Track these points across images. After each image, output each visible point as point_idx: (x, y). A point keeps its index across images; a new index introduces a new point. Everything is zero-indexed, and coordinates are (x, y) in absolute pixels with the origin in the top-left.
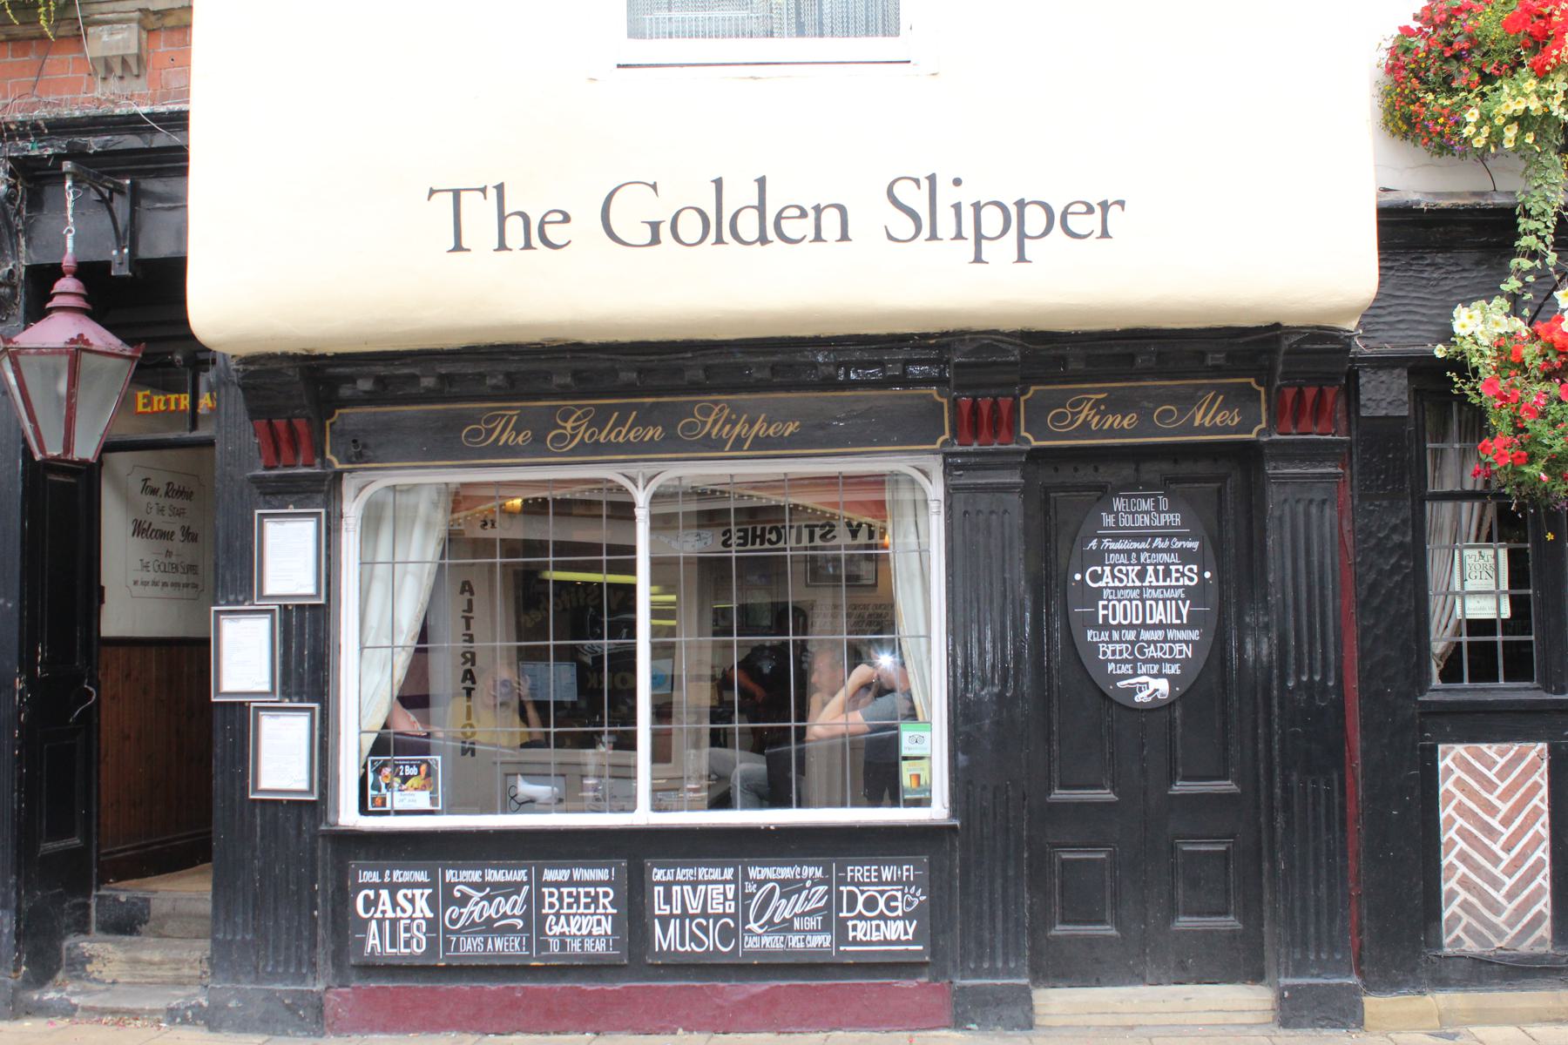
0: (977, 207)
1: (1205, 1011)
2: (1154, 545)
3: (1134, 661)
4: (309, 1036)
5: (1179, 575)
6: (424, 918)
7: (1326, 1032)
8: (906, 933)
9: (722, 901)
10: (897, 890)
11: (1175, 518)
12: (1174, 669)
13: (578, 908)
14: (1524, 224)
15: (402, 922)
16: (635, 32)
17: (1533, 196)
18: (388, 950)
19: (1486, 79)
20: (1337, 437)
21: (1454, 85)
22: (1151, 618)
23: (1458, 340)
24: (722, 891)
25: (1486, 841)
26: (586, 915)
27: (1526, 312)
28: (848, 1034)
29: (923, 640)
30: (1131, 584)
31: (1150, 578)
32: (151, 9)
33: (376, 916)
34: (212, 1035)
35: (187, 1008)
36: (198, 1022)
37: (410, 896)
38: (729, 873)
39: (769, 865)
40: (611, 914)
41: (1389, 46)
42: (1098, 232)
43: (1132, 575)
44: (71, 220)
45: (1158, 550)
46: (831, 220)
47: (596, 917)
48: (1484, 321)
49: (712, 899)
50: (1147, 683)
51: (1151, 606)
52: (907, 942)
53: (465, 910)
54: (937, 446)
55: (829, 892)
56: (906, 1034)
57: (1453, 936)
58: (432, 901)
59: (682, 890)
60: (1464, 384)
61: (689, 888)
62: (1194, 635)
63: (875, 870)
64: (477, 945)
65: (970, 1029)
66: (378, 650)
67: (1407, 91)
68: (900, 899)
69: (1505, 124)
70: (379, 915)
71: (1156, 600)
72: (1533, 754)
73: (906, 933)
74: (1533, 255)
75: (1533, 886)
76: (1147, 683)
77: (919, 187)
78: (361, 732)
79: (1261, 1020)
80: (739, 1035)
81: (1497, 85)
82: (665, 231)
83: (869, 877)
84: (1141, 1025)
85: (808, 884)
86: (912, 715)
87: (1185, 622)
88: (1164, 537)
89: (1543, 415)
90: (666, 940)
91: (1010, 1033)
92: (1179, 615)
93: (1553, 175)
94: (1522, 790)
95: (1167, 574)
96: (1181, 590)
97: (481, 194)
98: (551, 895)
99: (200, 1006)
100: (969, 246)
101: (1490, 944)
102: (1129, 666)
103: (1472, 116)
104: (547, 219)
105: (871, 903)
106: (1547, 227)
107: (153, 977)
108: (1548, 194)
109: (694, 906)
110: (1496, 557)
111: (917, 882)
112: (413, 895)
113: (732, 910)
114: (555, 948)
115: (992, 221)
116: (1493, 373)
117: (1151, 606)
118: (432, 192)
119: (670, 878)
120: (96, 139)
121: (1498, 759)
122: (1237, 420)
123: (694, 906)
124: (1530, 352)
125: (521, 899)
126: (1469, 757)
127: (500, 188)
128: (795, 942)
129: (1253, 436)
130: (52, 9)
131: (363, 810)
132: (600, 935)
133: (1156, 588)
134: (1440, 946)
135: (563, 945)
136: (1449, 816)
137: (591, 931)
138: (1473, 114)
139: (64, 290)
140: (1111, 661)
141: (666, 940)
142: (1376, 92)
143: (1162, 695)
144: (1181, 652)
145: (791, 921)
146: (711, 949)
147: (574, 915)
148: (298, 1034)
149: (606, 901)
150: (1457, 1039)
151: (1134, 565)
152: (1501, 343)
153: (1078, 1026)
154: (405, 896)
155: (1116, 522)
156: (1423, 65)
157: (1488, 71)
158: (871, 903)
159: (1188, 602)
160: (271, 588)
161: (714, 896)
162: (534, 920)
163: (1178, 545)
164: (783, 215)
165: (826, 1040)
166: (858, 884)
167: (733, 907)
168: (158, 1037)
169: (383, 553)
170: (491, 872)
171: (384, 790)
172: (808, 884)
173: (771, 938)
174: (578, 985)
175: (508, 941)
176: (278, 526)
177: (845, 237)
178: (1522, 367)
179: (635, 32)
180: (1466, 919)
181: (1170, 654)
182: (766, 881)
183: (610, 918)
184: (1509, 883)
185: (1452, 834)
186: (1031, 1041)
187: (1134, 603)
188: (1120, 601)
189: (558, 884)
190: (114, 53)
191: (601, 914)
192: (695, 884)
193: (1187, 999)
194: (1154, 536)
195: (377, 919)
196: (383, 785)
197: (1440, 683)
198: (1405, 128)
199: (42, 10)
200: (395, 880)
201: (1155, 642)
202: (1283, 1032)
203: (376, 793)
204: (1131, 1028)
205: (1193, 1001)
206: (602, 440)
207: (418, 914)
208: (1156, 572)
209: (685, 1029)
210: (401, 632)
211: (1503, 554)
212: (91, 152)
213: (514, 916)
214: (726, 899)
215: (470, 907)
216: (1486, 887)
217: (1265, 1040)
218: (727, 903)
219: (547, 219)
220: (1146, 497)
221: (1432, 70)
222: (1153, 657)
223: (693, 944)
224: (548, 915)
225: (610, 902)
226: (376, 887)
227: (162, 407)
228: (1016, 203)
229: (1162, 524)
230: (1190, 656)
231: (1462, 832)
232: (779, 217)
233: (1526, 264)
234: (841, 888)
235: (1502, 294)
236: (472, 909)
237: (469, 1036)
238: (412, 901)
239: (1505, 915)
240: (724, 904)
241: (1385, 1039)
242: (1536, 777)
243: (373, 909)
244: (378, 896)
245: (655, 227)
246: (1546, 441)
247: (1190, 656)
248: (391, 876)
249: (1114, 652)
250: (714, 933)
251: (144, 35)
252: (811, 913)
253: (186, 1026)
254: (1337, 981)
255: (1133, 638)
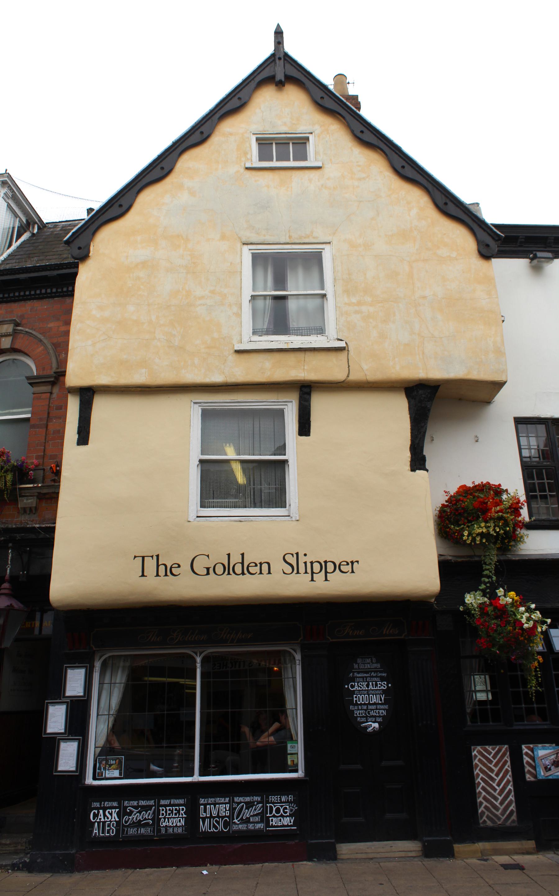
0: (312, 563)
1: (398, 852)
2: (372, 675)
3: (367, 717)
4: (68, 873)
5: (380, 685)
6: (115, 821)
7: (441, 859)
8: (290, 822)
9: (224, 811)
10: (287, 805)
11: (379, 666)
12: (380, 720)
13: (172, 815)
14: (485, 567)
15: (107, 823)
16: (202, 506)
17: (487, 558)
18: (101, 835)
19: (469, 521)
20: (430, 637)
21: (460, 523)
22: (372, 701)
23: (467, 605)
24: (224, 807)
25: (491, 782)
26: (175, 818)
27: (488, 596)
28: (270, 864)
29: (294, 710)
30: (364, 689)
31: (371, 687)
32: (42, 492)
33: (97, 821)
34: (29, 874)
35: (20, 863)
36: (24, 869)
37: (110, 812)
38: (227, 800)
39: (242, 796)
40: (184, 817)
41: (438, 510)
42: (350, 571)
43: (365, 686)
44: (9, 563)
45: (373, 677)
46: (265, 567)
47: (178, 819)
48: (475, 599)
49: (221, 810)
50: (371, 725)
51: (371, 696)
52: (291, 826)
53: (131, 817)
54: (299, 641)
55: (263, 807)
56: (291, 863)
57: (483, 820)
58: (118, 814)
59: (210, 807)
60: (470, 619)
61: (213, 806)
62: (386, 707)
63: (279, 798)
64: (135, 831)
65: (314, 861)
66: (103, 716)
67: (445, 525)
68: (288, 809)
69: (476, 536)
70: (98, 820)
71: (373, 695)
72: (504, 749)
73: (290, 822)
74: (488, 577)
75: (509, 799)
76: (371, 725)
77: (293, 557)
78: (95, 747)
79: (418, 855)
80: (230, 866)
81: (473, 523)
82: (211, 570)
83: (277, 800)
84: (375, 858)
85: (255, 803)
86: (291, 739)
87: (383, 702)
88: (375, 672)
89: (496, 631)
90: (204, 827)
91: (328, 862)
92: (381, 700)
93: (493, 551)
94: (501, 763)
95: (376, 685)
96: (381, 691)
97: (151, 558)
98: (163, 810)
99: (25, 861)
100: (309, 575)
101: (496, 823)
102: (365, 719)
103: (466, 533)
104: (173, 566)
105: (278, 811)
106: (492, 568)
107: (6, 850)
108: (491, 557)
109: (215, 813)
110: (485, 678)
111: (294, 802)
112: (112, 812)
113: (228, 815)
114: (163, 831)
115: (317, 567)
116: (479, 616)
117: (371, 696)
118: (135, 557)
119: (206, 802)
120: (19, 535)
121: (492, 751)
122: (397, 632)
123: (215, 813)
124: (490, 609)
125: (151, 812)
126: (482, 751)
127: (158, 556)
128: (251, 826)
129: (402, 637)
130: (9, 492)
131: (94, 778)
132: (180, 826)
133: (373, 690)
134: (479, 824)
135: (166, 830)
136: (477, 773)
137: (177, 824)
138: (466, 533)
139: (5, 587)
140: (359, 717)
141: (204, 827)
142: (435, 524)
143: (377, 729)
144: (382, 713)
145: (249, 818)
146: (220, 830)
147: (171, 818)
148: (64, 872)
149: (183, 812)
150: (488, 861)
151: (365, 682)
152: (481, 606)
153: (353, 859)
154: (109, 812)
155: (359, 667)
156: (450, 517)
157: (469, 519)
158: (278, 811)
159: (384, 695)
160: (68, 693)
161: (222, 809)
162: (156, 820)
163: (380, 675)
164: (250, 565)
165: (262, 867)
166: (273, 803)
167: (228, 813)
168: (8, 876)
169: (107, 680)
170: (141, 801)
171: (102, 770)
172: (255, 803)
173: (242, 825)
174: (171, 847)
175: (146, 829)
176: (72, 671)
177: (269, 573)
178: (487, 614)
179: (202, 506)
180: (487, 813)
181: (379, 714)
182: (241, 802)
183: (184, 819)
184: (500, 798)
185: (479, 780)
186: (336, 865)
187: (366, 695)
188: (361, 695)
189: (165, 806)
190: (28, 506)
191: (180, 817)
192: (215, 805)
193: (391, 847)
194: (371, 672)
195: (98, 822)
196: (102, 768)
197: (470, 724)
198: (445, 536)
199: (6, 492)
200: (105, 805)
201: (373, 710)
202: (426, 859)
203: (99, 771)
204: (372, 859)
205: (393, 847)
206: (186, 640)
207: (113, 819)
208: (373, 684)
209: (210, 864)
210: (113, 709)
211: (487, 677)
212: (17, 539)
213: (149, 819)
214: (226, 810)
215: (133, 816)
216: (493, 800)
217: (420, 863)
218: (226, 812)
219: (173, 566)
220: (368, 658)
221: (452, 518)
222: (373, 715)
223: (214, 829)
224: (161, 818)
225: (184, 812)
226: (98, 809)
227: (29, 626)
228: (324, 562)
229: (374, 667)
230: (385, 714)
231: (482, 779)
232: (248, 566)
233: (487, 580)
234: (267, 805)
235: (480, 590)
236: (133, 817)
237: (129, 870)
238: (111, 814)
239: (500, 811)
240: (225, 812)
241: (462, 862)
242: (506, 758)
243: (96, 818)
244: (98, 812)
245: (208, 569)
246: (497, 640)
247: (385, 714)
248: (104, 804)
249: (359, 714)
250: (222, 824)
251: (38, 500)
252: (257, 815)
253: (18, 871)
254: (444, 838)
255: (366, 708)
